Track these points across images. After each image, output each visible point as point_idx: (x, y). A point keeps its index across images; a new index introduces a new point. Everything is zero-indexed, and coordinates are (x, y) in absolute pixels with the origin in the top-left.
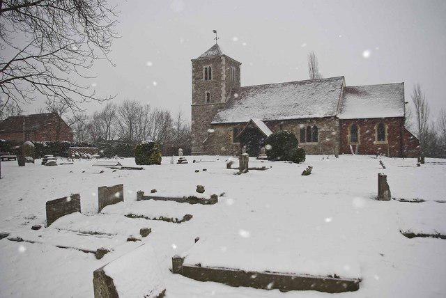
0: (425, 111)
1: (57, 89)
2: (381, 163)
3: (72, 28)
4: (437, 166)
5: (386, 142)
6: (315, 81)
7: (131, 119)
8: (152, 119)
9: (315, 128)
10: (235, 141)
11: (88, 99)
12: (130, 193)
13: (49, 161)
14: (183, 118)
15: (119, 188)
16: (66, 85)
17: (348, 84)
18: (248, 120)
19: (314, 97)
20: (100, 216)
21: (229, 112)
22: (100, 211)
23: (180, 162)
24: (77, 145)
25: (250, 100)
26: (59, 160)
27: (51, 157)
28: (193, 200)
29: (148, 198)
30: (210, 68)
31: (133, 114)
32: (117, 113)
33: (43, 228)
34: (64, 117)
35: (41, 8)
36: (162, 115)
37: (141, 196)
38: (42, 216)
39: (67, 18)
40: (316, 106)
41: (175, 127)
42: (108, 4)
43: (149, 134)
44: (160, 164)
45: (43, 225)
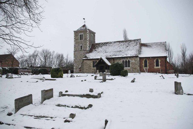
0: (171, 54)
1: (16, 43)
2: (162, 76)
3: (22, 14)
4: (184, 77)
5: (160, 67)
6: (126, 41)
7: (45, 57)
8: (55, 57)
9: (129, 61)
10: (94, 67)
11: (30, 47)
12: (56, 93)
13: (9, 76)
14: (69, 57)
15: (51, 90)
16: (19, 40)
17: (142, 42)
18: (100, 58)
19: (128, 48)
20: (42, 106)
21: (91, 54)
22: (42, 103)
23: (71, 76)
24: (22, 69)
25: (100, 49)
26: (14, 76)
27: (10, 74)
28: (88, 96)
29: (65, 95)
30: (82, 35)
31: (47, 55)
32: (39, 55)
33: (14, 114)
34: (15, 56)
35: (7, 5)
36: (59, 56)
37: (61, 95)
38: (12, 106)
39: (20, 9)
40: (129, 52)
41: (65, 61)
42: (39, 4)
43: (54, 64)
44: (62, 77)
45: (13, 112)
